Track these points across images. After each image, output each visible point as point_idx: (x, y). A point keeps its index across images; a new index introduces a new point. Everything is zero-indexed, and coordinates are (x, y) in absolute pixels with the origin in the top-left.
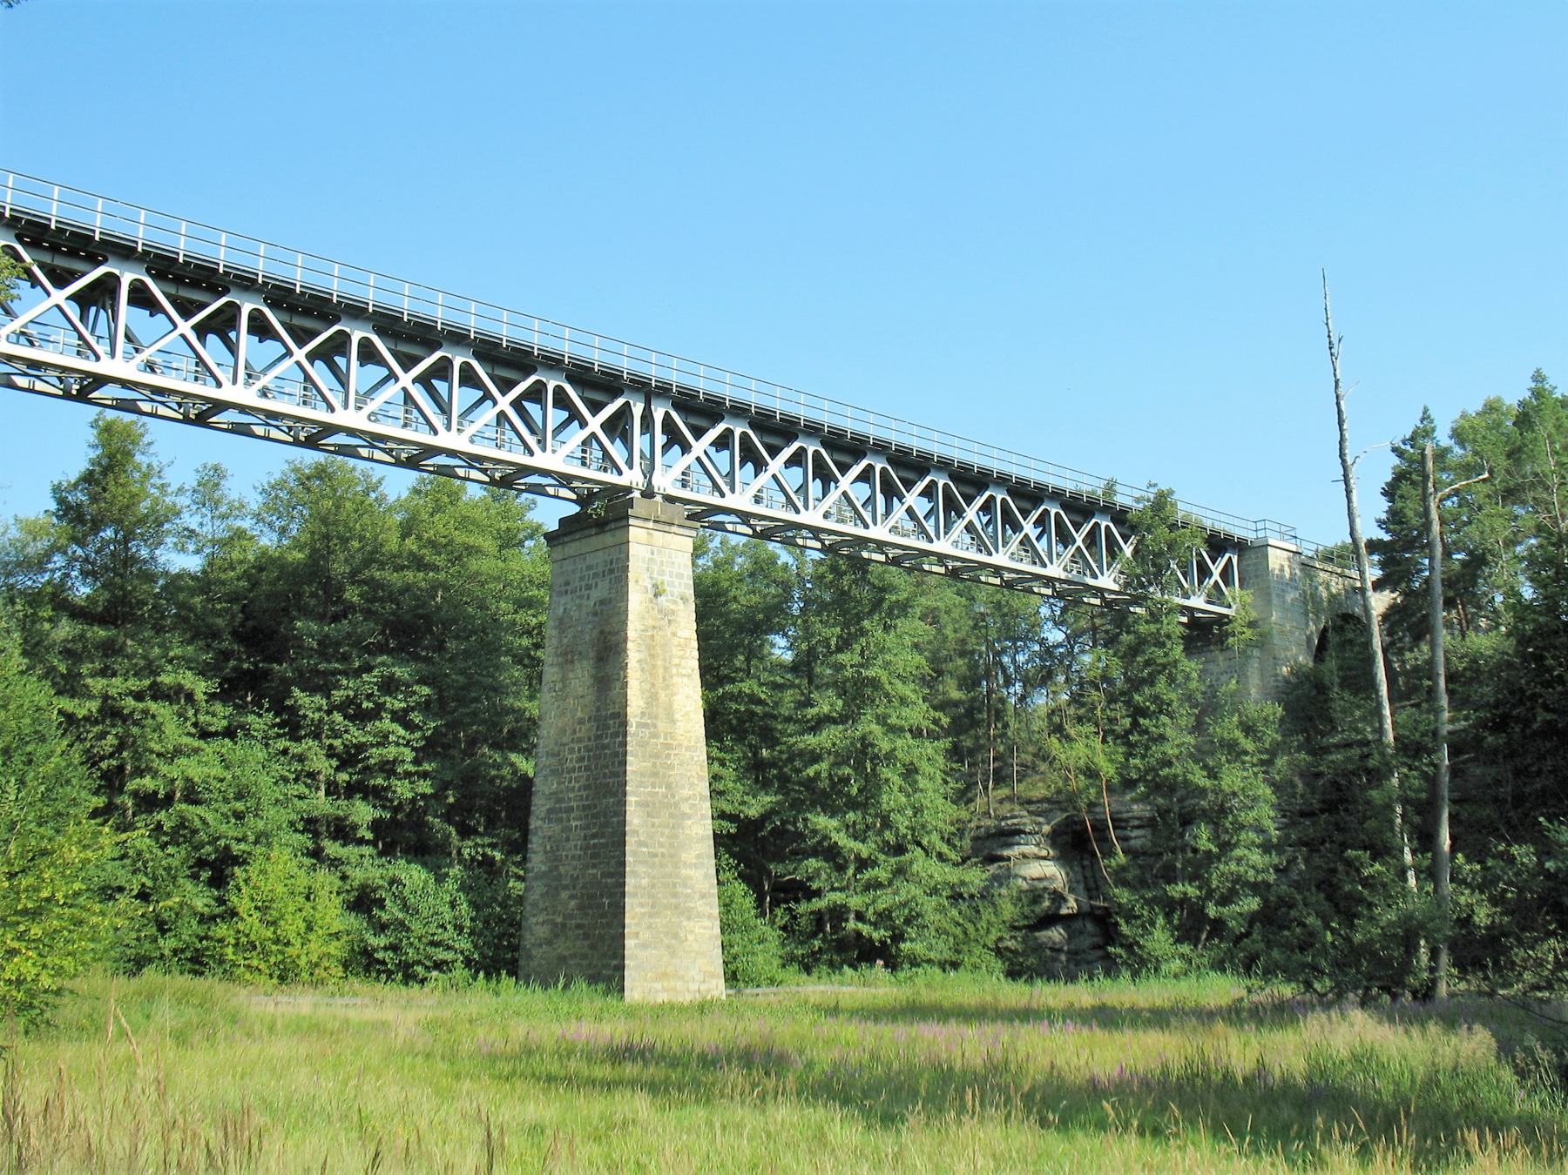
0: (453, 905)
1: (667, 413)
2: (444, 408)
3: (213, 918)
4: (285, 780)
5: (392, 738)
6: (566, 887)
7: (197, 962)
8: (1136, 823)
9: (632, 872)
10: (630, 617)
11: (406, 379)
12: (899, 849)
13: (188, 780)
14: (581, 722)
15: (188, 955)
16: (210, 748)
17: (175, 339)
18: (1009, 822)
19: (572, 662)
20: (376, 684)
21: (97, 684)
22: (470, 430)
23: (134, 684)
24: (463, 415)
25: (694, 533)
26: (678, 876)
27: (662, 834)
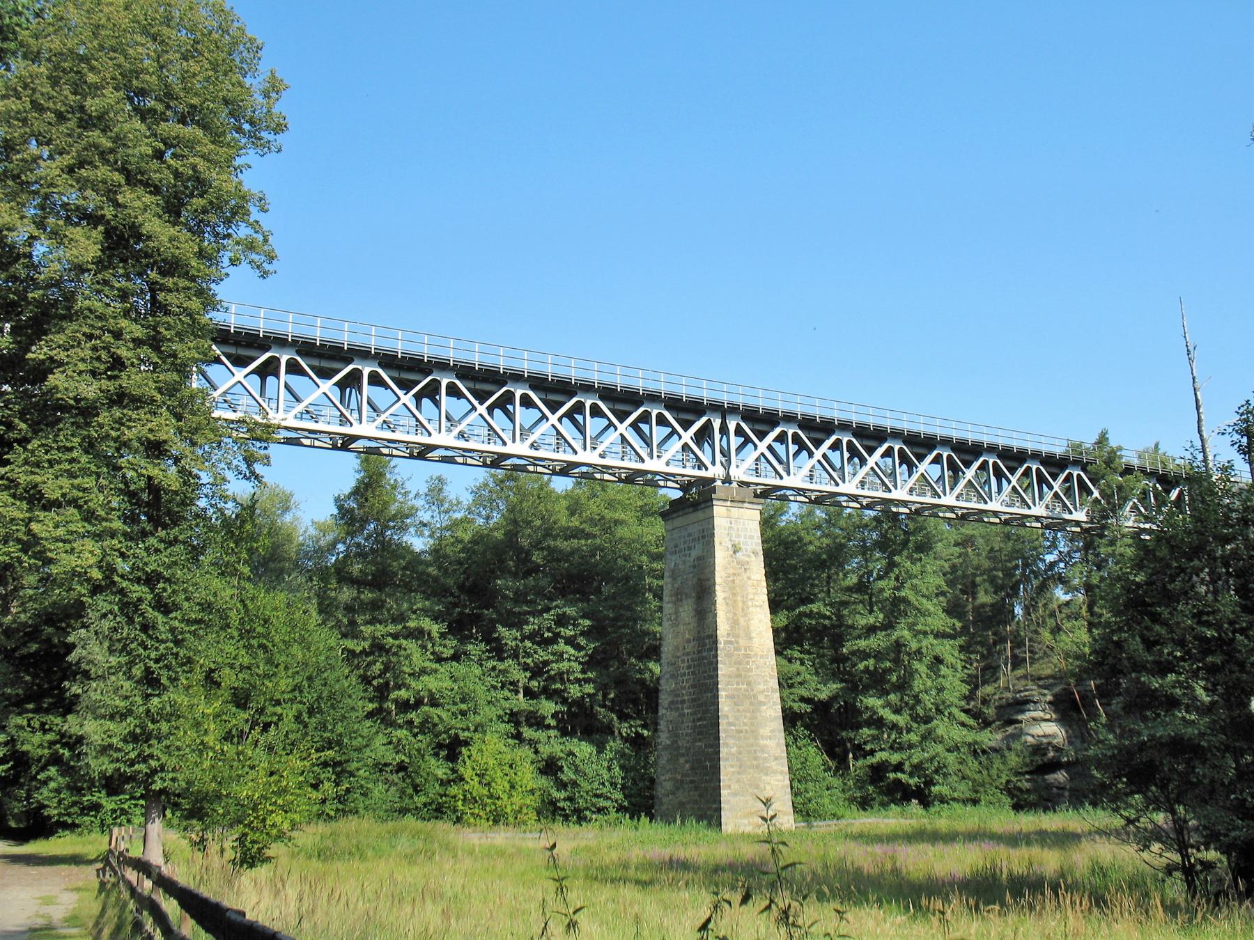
0: (609, 769)
1: (738, 424)
2: (647, 441)
3: (449, 782)
4: (495, 688)
5: (565, 656)
6: (683, 755)
7: (438, 811)
9: (724, 744)
11: (553, 419)
12: (928, 720)
13: (430, 691)
14: (688, 641)
15: (434, 807)
16: (444, 669)
17: (307, 397)
18: (1022, 694)
19: (681, 600)
20: (553, 620)
21: (367, 630)
22: (666, 457)
23: (392, 628)
24: (660, 445)
25: (760, 507)
26: (758, 745)
27: (745, 717)
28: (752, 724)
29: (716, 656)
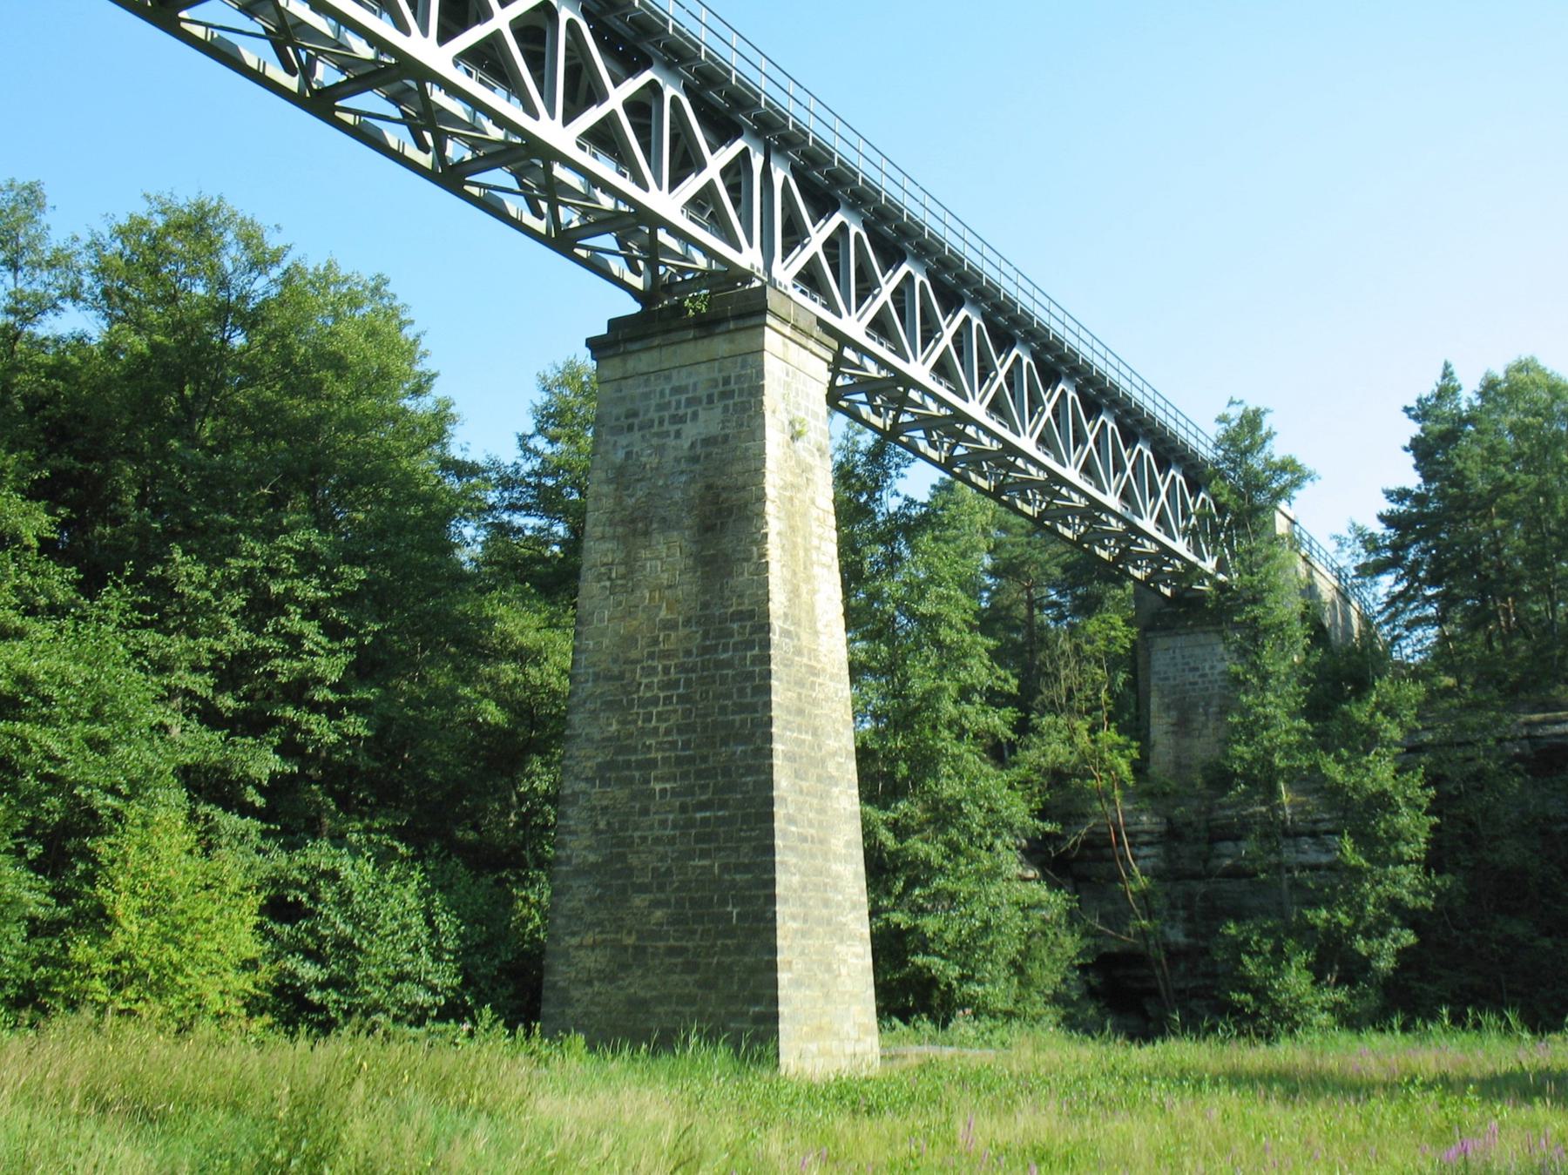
6: (643, 889)
8: (1146, 838)
10: (768, 464)
14: (669, 626)
29: (767, 660)
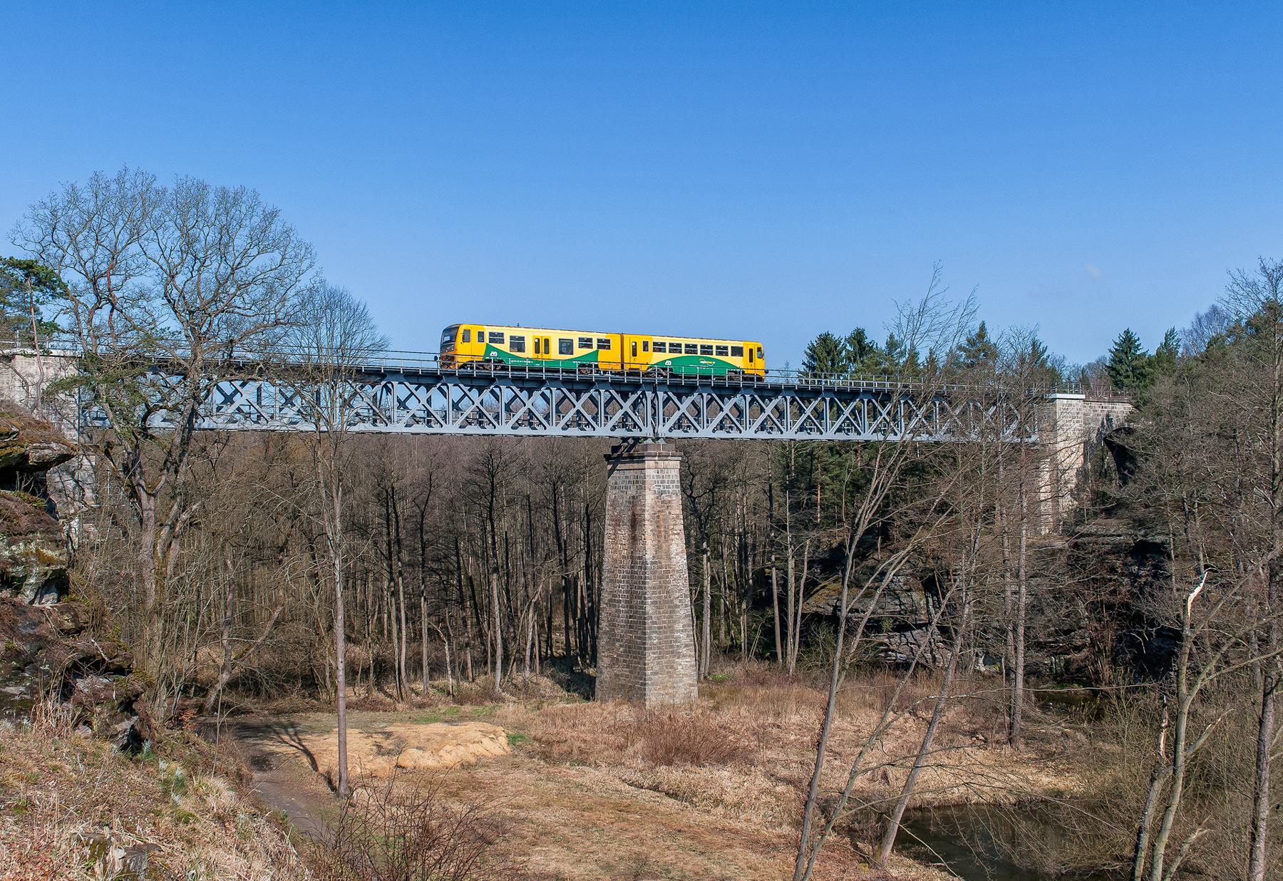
6: (618, 640)
26: (673, 637)
28: (669, 622)
